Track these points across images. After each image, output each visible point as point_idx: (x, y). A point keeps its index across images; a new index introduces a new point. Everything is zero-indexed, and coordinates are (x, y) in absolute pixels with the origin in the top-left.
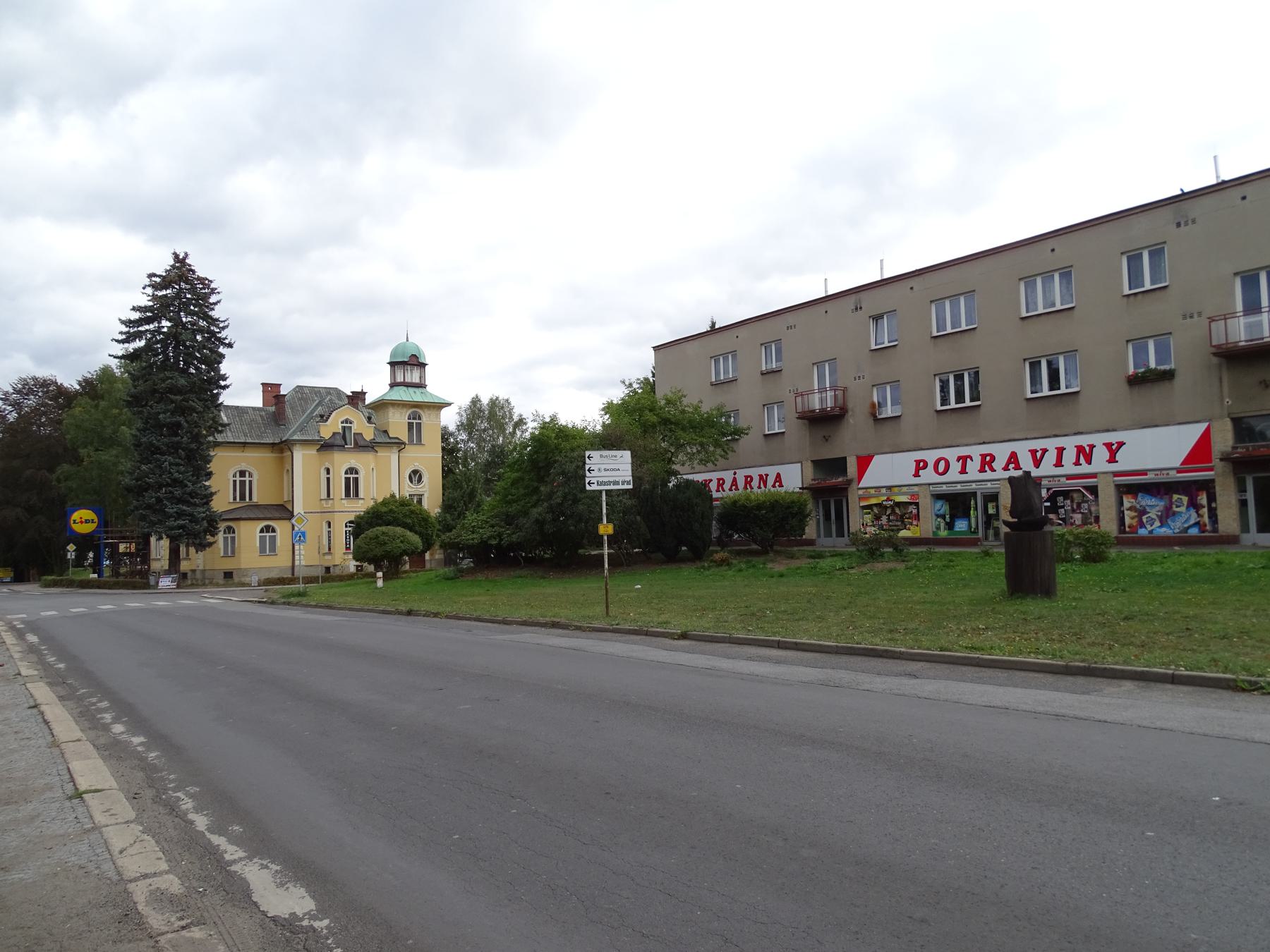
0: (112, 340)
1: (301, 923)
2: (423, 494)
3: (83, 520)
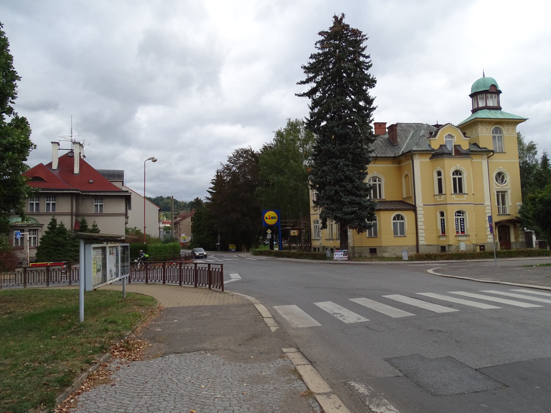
0: (297, 84)
2: (507, 191)
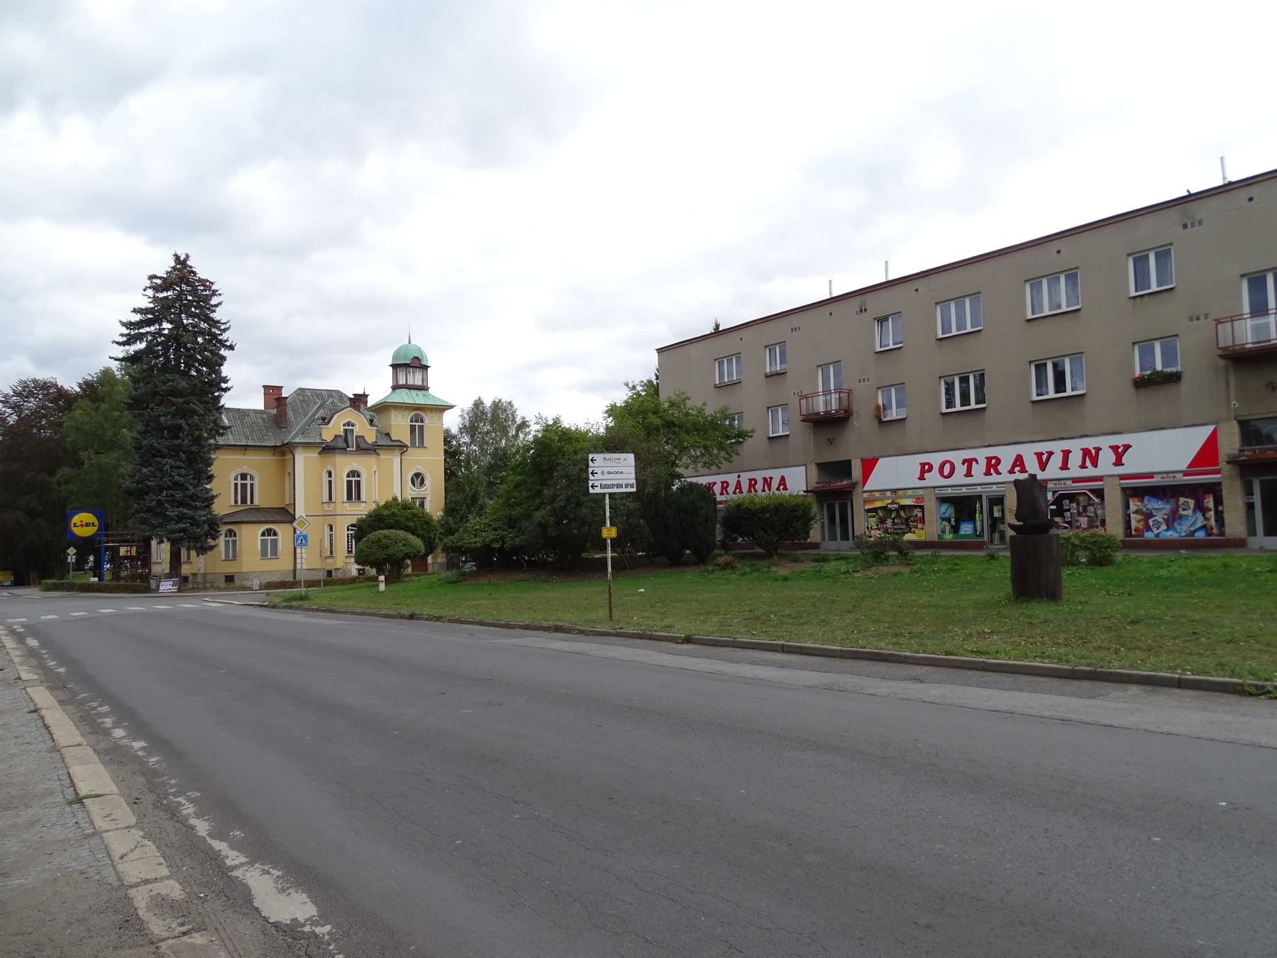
0: (112, 342)
2: (426, 498)
3: (83, 523)
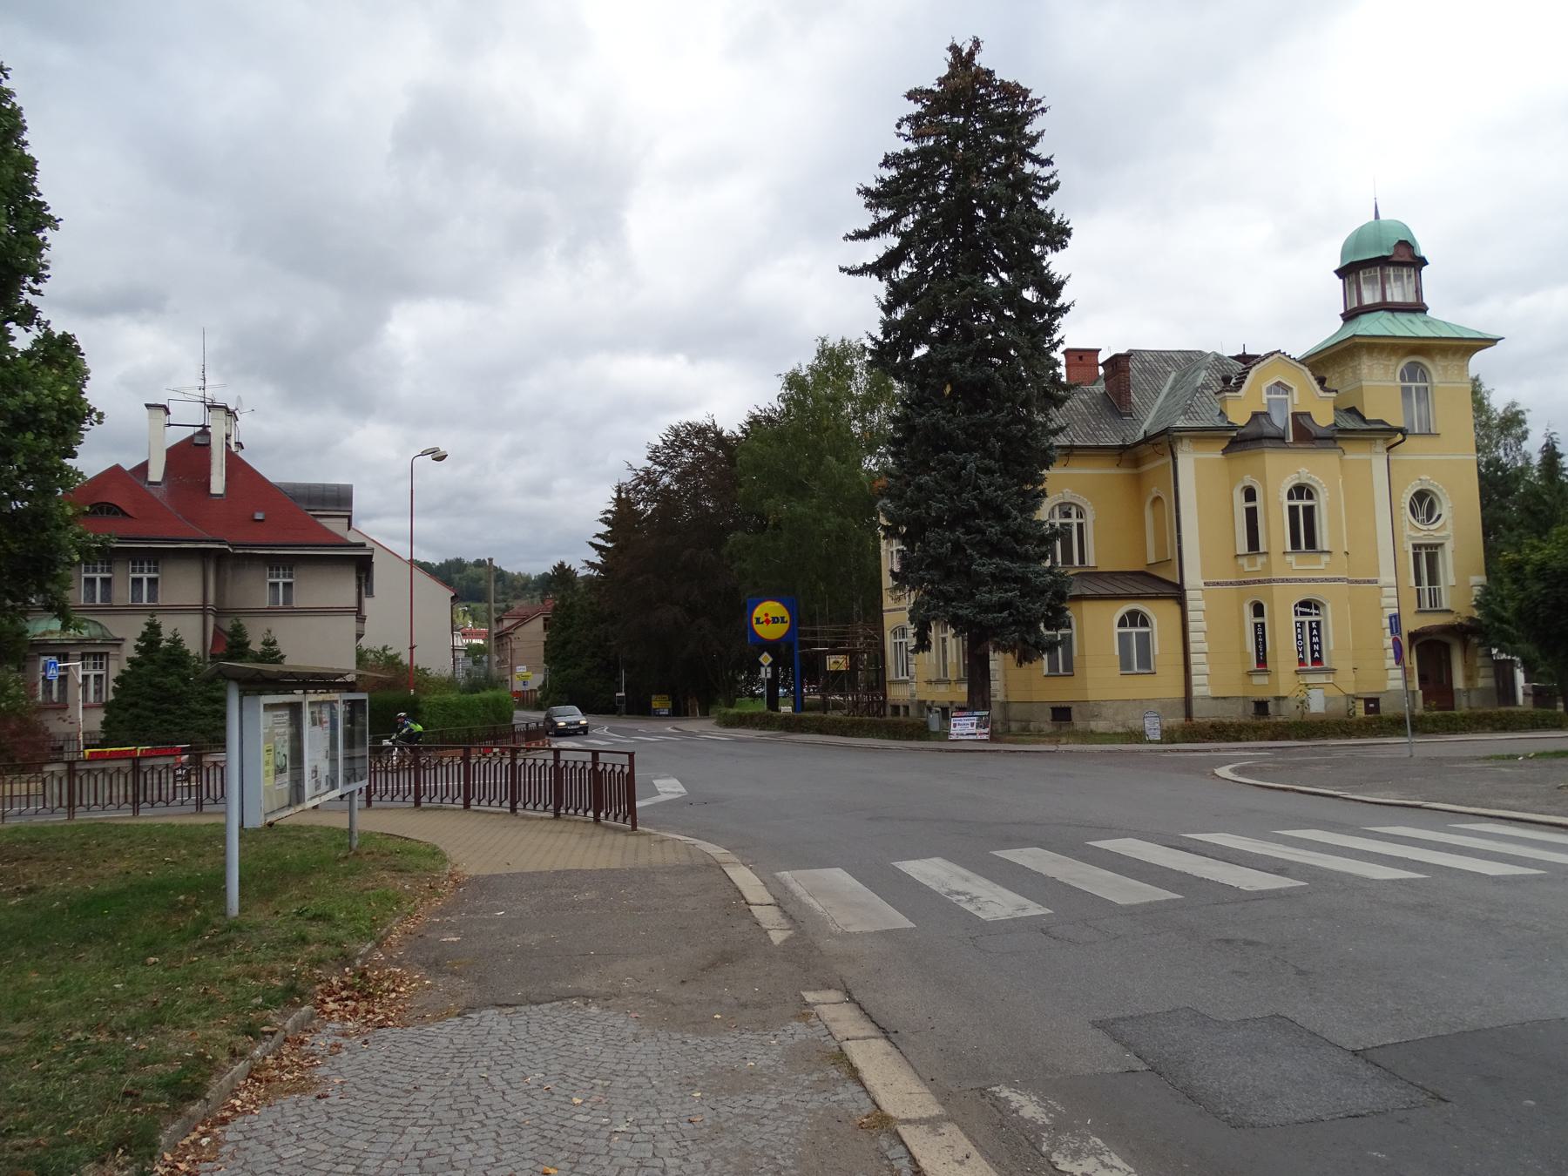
0: (845, 239)
1: (465, 574)
2: (1441, 545)
